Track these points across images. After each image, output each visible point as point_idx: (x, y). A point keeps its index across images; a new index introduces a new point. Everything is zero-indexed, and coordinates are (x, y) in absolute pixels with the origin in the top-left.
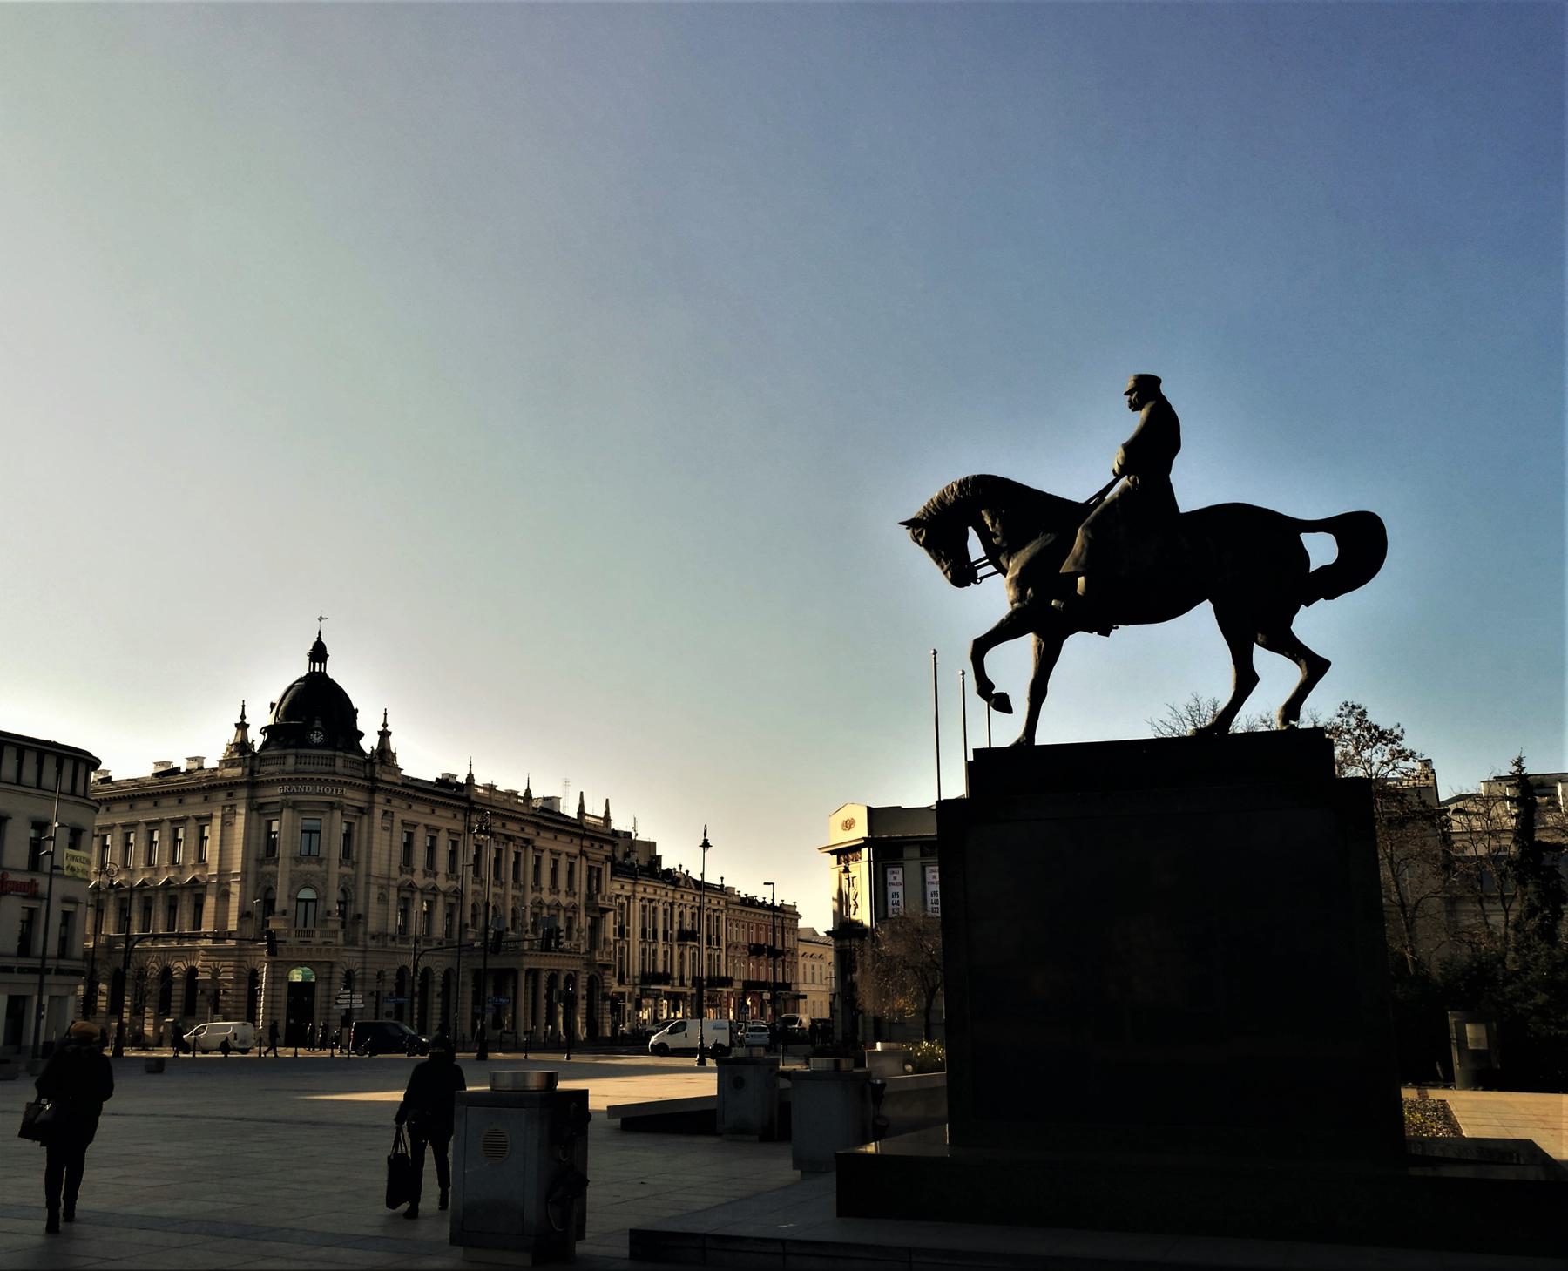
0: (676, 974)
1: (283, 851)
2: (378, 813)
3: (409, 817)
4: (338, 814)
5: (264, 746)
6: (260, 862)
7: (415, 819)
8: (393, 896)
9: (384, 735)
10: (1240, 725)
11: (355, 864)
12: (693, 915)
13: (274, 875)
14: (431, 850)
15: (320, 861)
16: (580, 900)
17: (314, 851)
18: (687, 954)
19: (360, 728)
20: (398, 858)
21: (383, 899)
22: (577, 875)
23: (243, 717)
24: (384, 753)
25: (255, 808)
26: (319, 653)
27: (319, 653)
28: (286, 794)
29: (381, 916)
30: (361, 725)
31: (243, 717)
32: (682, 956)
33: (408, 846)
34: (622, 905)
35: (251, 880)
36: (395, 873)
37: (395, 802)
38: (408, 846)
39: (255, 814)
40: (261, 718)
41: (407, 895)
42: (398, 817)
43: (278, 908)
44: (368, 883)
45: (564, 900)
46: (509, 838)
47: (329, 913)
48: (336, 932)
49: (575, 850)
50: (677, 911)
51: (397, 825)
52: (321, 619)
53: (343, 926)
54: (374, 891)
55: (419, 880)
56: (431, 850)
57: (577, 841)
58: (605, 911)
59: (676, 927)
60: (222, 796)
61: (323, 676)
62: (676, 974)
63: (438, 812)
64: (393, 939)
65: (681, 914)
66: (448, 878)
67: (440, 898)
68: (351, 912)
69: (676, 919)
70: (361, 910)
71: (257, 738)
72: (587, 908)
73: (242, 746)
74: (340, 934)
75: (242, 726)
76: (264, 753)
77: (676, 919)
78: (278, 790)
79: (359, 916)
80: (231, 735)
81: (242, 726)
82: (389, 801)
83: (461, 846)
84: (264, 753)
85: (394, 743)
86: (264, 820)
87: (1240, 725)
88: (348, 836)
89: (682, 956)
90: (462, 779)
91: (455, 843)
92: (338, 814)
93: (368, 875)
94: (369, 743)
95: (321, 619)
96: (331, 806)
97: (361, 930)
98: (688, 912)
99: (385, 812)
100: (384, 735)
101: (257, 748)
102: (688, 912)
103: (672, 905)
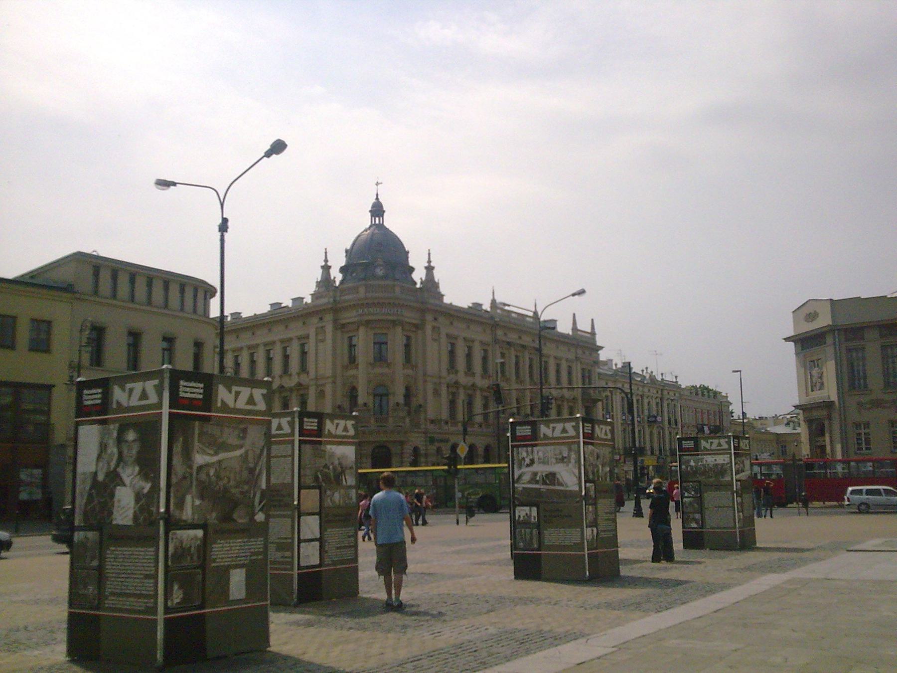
0: (648, 447)
1: (361, 359)
2: (429, 328)
3: (453, 331)
4: (399, 330)
5: (342, 282)
6: (345, 368)
7: (456, 333)
8: (444, 391)
9: (430, 269)
10: (67, 550)
11: (414, 367)
12: (657, 403)
13: (355, 377)
14: (469, 356)
15: (388, 365)
16: (578, 394)
17: (378, 398)
18: (655, 431)
19: (411, 264)
20: (445, 365)
21: (436, 393)
22: (574, 374)
23: (326, 261)
24: (431, 284)
25: (340, 327)
26: (377, 210)
27: (377, 210)
28: (361, 315)
29: (435, 407)
30: (412, 262)
31: (326, 261)
32: (651, 434)
33: (452, 353)
34: (607, 396)
35: (339, 381)
36: (444, 373)
37: (441, 319)
38: (452, 353)
39: (339, 333)
40: (338, 261)
41: (454, 390)
42: (444, 331)
43: (360, 401)
44: (425, 381)
45: (567, 394)
46: (523, 347)
47: (398, 404)
48: (404, 418)
49: (571, 356)
50: (646, 401)
51: (444, 339)
52: (377, 184)
53: (409, 413)
54: (430, 387)
55: (463, 379)
56: (469, 356)
57: (573, 350)
58: (595, 401)
59: (646, 412)
60: (315, 320)
61: (381, 226)
62: (648, 447)
63: (472, 327)
64: (447, 423)
65: (649, 403)
66: (483, 377)
67: (478, 393)
68: (414, 403)
69: (646, 407)
70: (421, 402)
71: (337, 276)
72: (582, 400)
73: (326, 282)
74: (408, 420)
75: (326, 268)
76: (345, 286)
77: (646, 407)
78: (354, 313)
79: (420, 406)
80: (318, 275)
81: (326, 268)
82: (321, 319)
83: (490, 352)
84: (345, 286)
85: (437, 275)
86: (346, 336)
87: (67, 550)
88: (407, 346)
89: (651, 434)
90: (487, 306)
91: (486, 351)
92: (399, 330)
93: (425, 375)
94: (419, 276)
95: (377, 184)
96: (394, 323)
97: (422, 416)
98: (653, 403)
99: (434, 328)
100: (430, 269)
101: (337, 284)
102: (653, 403)
103: (642, 396)
